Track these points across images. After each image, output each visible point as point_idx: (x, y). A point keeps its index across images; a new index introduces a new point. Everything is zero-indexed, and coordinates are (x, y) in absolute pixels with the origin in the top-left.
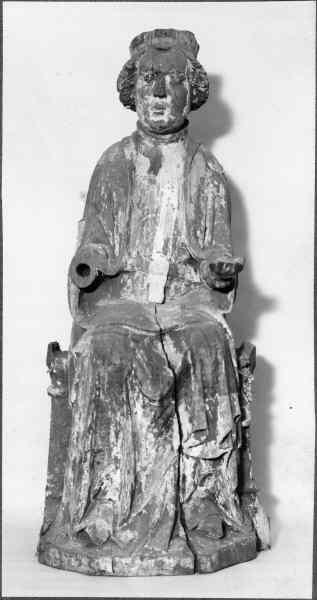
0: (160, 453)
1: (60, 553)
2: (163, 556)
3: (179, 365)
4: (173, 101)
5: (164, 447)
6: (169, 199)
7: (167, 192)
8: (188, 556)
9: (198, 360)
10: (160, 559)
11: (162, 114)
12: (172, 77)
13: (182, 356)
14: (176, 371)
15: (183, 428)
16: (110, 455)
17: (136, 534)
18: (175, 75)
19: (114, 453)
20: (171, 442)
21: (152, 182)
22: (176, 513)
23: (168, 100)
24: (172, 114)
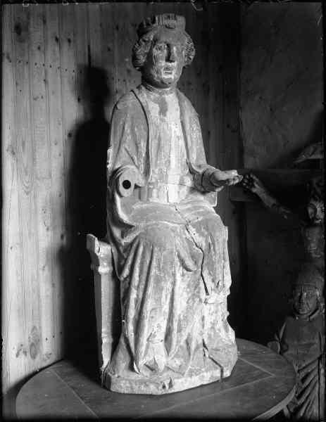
0: (191, 305)
1: (130, 383)
2: (203, 372)
3: (204, 245)
4: (178, 65)
5: (193, 299)
6: (175, 132)
7: (173, 127)
8: (217, 368)
9: (215, 240)
10: (201, 374)
11: (171, 73)
12: (177, 48)
13: (205, 239)
14: (203, 249)
15: (208, 286)
16: (160, 311)
17: (182, 360)
18: (179, 47)
19: (163, 309)
20: (199, 297)
21: (162, 120)
22: (127, 277)
23: (175, 64)
24: (176, 74)
